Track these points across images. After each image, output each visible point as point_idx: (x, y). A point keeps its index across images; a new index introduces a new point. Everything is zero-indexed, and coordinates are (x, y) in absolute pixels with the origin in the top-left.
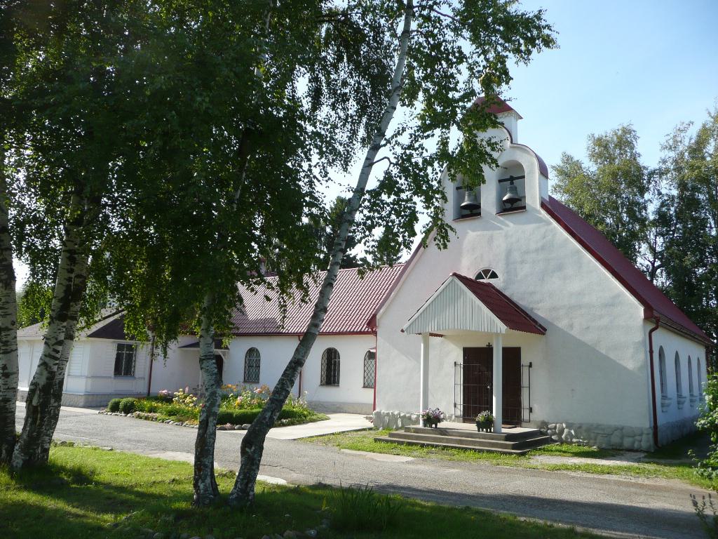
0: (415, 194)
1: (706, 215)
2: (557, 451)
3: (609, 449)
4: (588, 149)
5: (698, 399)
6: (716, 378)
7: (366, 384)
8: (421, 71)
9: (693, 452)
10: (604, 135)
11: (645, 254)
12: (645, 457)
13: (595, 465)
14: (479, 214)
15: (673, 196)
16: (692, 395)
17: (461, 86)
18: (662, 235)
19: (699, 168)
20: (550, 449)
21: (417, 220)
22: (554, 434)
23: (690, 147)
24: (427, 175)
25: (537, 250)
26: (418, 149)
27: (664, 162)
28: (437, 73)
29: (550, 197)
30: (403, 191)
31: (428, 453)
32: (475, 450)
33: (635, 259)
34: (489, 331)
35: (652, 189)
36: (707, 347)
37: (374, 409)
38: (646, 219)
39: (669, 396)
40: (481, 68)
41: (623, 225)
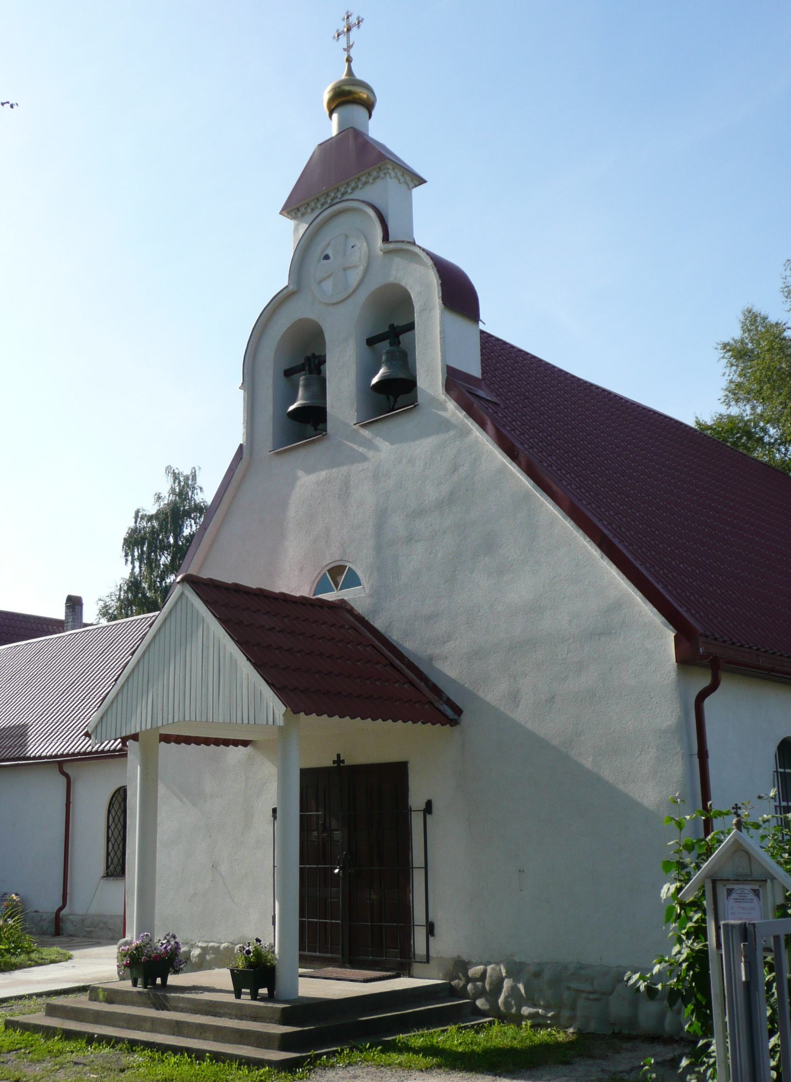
22: (481, 993)
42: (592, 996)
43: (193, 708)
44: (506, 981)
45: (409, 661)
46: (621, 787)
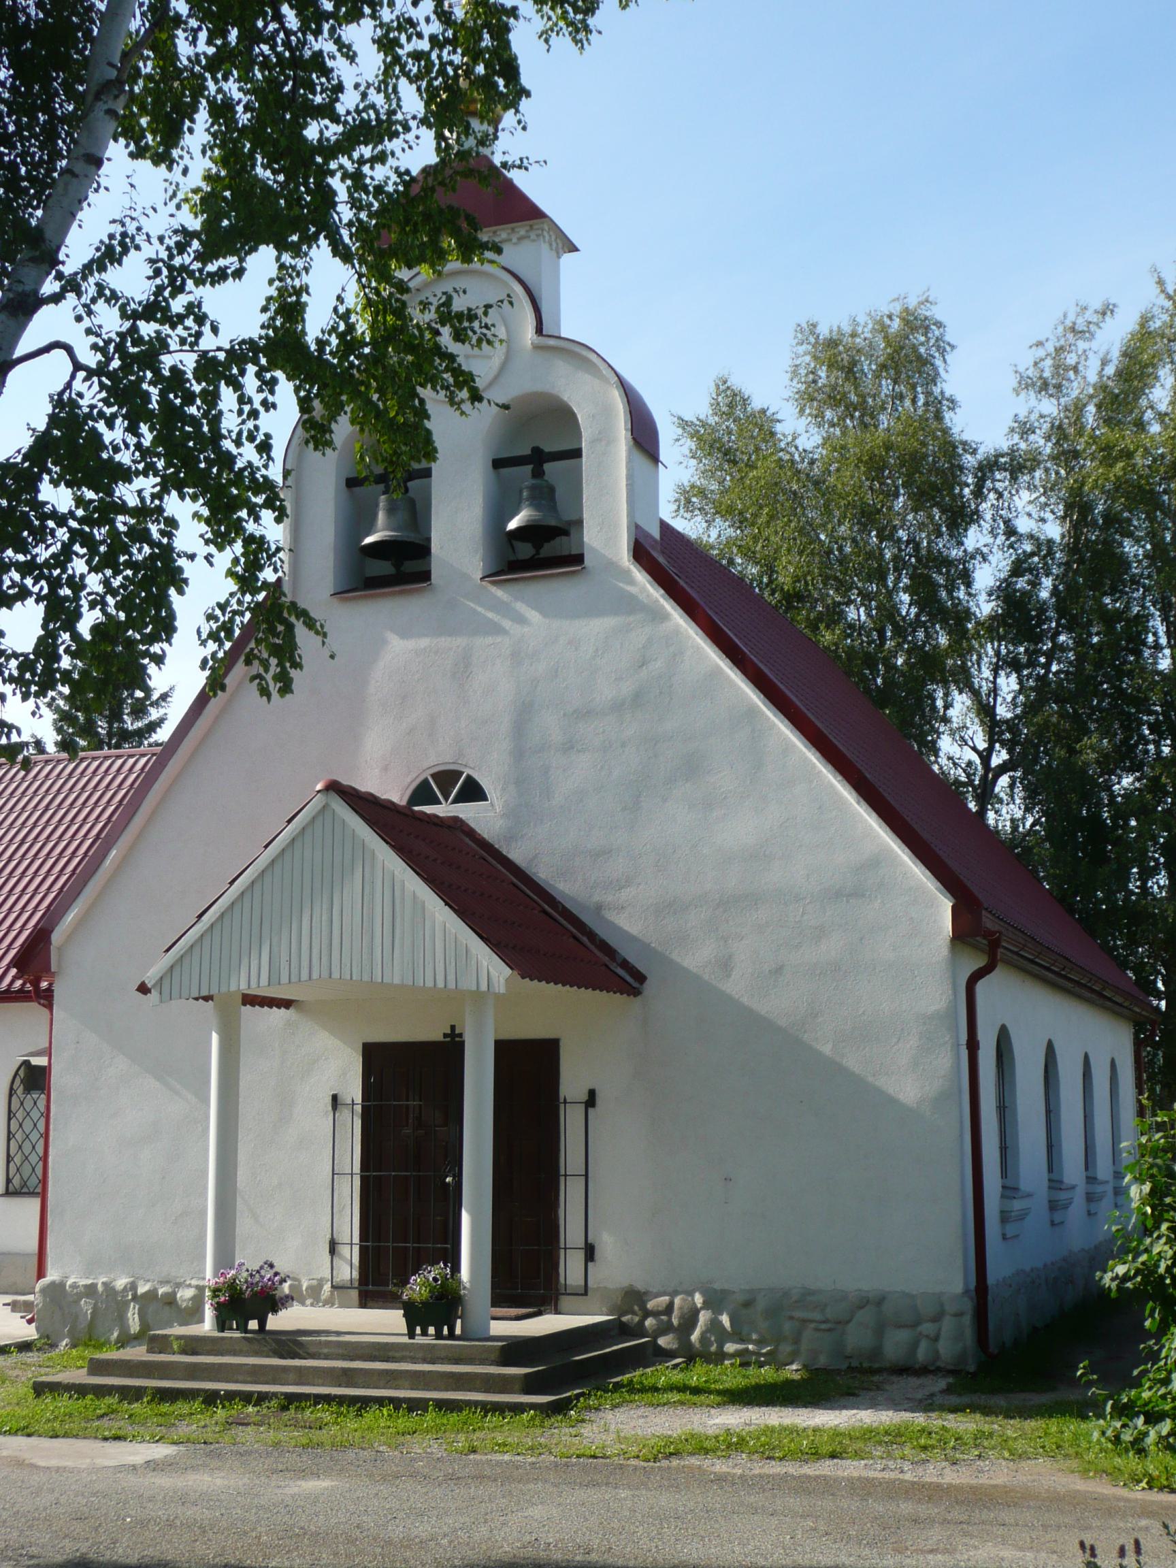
0: (167, 485)
1: (1144, 607)
2: (672, 1388)
3: (838, 1372)
4: (795, 372)
5: (1109, 1189)
6: (1160, 1127)
7: (16, 1181)
8: (203, 36)
9: (1091, 1369)
10: (847, 329)
11: (965, 727)
12: (949, 1390)
13: (793, 1431)
14: (425, 576)
15: (1050, 542)
16: (1091, 1180)
17: (348, 101)
18: (1015, 665)
19: (1128, 455)
20: (647, 1382)
21: (180, 583)
22: (666, 1329)
23: (1104, 388)
24: (215, 421)
25: (618, 707)
26: (181, 318)
27: (1025, 430)
28: (265, 48)
29: (665, 527)
30: (126, 475)
31: (229, 1424)
32: (396, 1403)
33: (934, 742)
34: (452, 985)
35: (988, 516)
36: (1138, 1027)
37: (41, 1274)
38: (967, 614)
39: (1024, 1186)
40: (424, 45)
41: (899, 632)
42: (823, 1326)
43: (346, 960)
44: (702, 1313)
45: (564, 907)
46: (870, 1079)
